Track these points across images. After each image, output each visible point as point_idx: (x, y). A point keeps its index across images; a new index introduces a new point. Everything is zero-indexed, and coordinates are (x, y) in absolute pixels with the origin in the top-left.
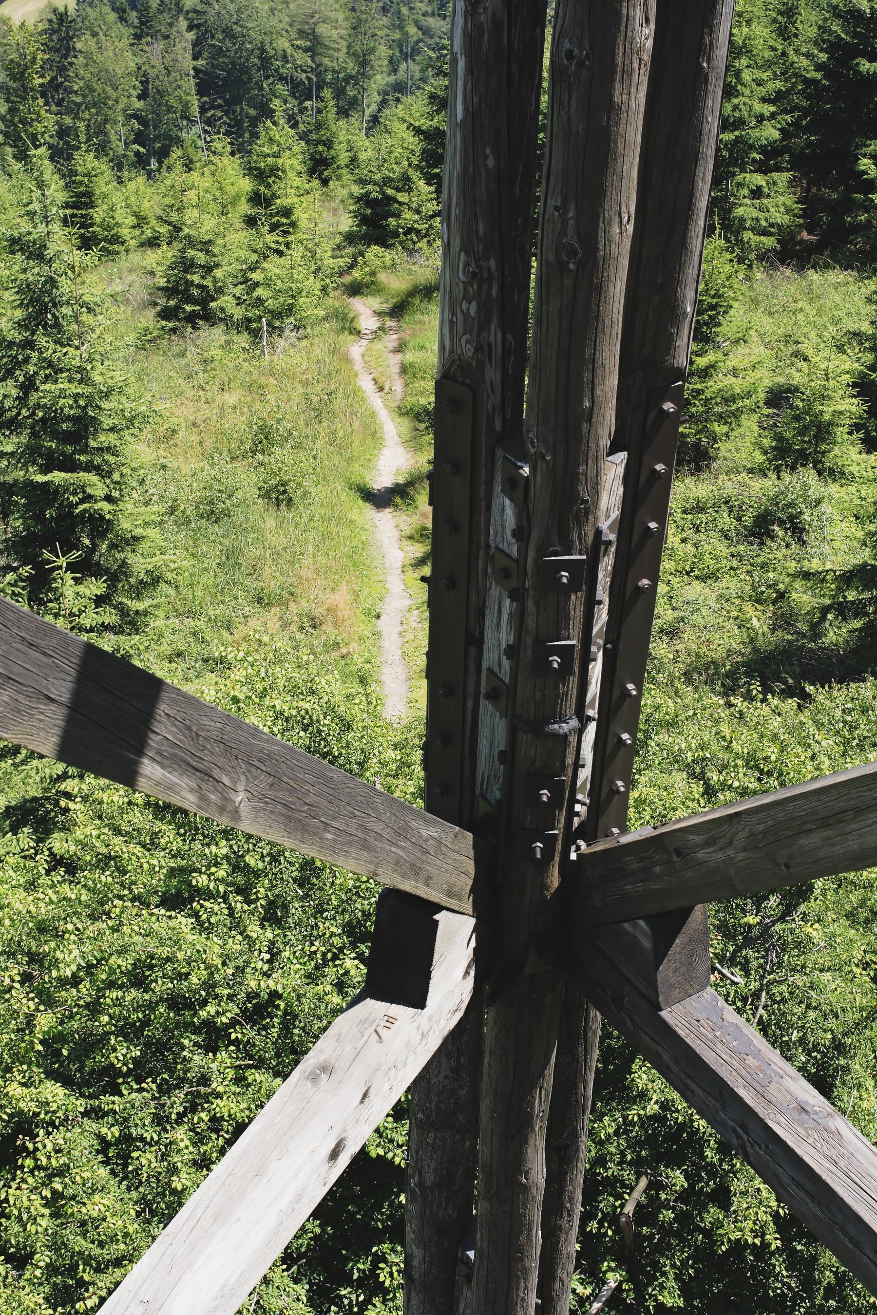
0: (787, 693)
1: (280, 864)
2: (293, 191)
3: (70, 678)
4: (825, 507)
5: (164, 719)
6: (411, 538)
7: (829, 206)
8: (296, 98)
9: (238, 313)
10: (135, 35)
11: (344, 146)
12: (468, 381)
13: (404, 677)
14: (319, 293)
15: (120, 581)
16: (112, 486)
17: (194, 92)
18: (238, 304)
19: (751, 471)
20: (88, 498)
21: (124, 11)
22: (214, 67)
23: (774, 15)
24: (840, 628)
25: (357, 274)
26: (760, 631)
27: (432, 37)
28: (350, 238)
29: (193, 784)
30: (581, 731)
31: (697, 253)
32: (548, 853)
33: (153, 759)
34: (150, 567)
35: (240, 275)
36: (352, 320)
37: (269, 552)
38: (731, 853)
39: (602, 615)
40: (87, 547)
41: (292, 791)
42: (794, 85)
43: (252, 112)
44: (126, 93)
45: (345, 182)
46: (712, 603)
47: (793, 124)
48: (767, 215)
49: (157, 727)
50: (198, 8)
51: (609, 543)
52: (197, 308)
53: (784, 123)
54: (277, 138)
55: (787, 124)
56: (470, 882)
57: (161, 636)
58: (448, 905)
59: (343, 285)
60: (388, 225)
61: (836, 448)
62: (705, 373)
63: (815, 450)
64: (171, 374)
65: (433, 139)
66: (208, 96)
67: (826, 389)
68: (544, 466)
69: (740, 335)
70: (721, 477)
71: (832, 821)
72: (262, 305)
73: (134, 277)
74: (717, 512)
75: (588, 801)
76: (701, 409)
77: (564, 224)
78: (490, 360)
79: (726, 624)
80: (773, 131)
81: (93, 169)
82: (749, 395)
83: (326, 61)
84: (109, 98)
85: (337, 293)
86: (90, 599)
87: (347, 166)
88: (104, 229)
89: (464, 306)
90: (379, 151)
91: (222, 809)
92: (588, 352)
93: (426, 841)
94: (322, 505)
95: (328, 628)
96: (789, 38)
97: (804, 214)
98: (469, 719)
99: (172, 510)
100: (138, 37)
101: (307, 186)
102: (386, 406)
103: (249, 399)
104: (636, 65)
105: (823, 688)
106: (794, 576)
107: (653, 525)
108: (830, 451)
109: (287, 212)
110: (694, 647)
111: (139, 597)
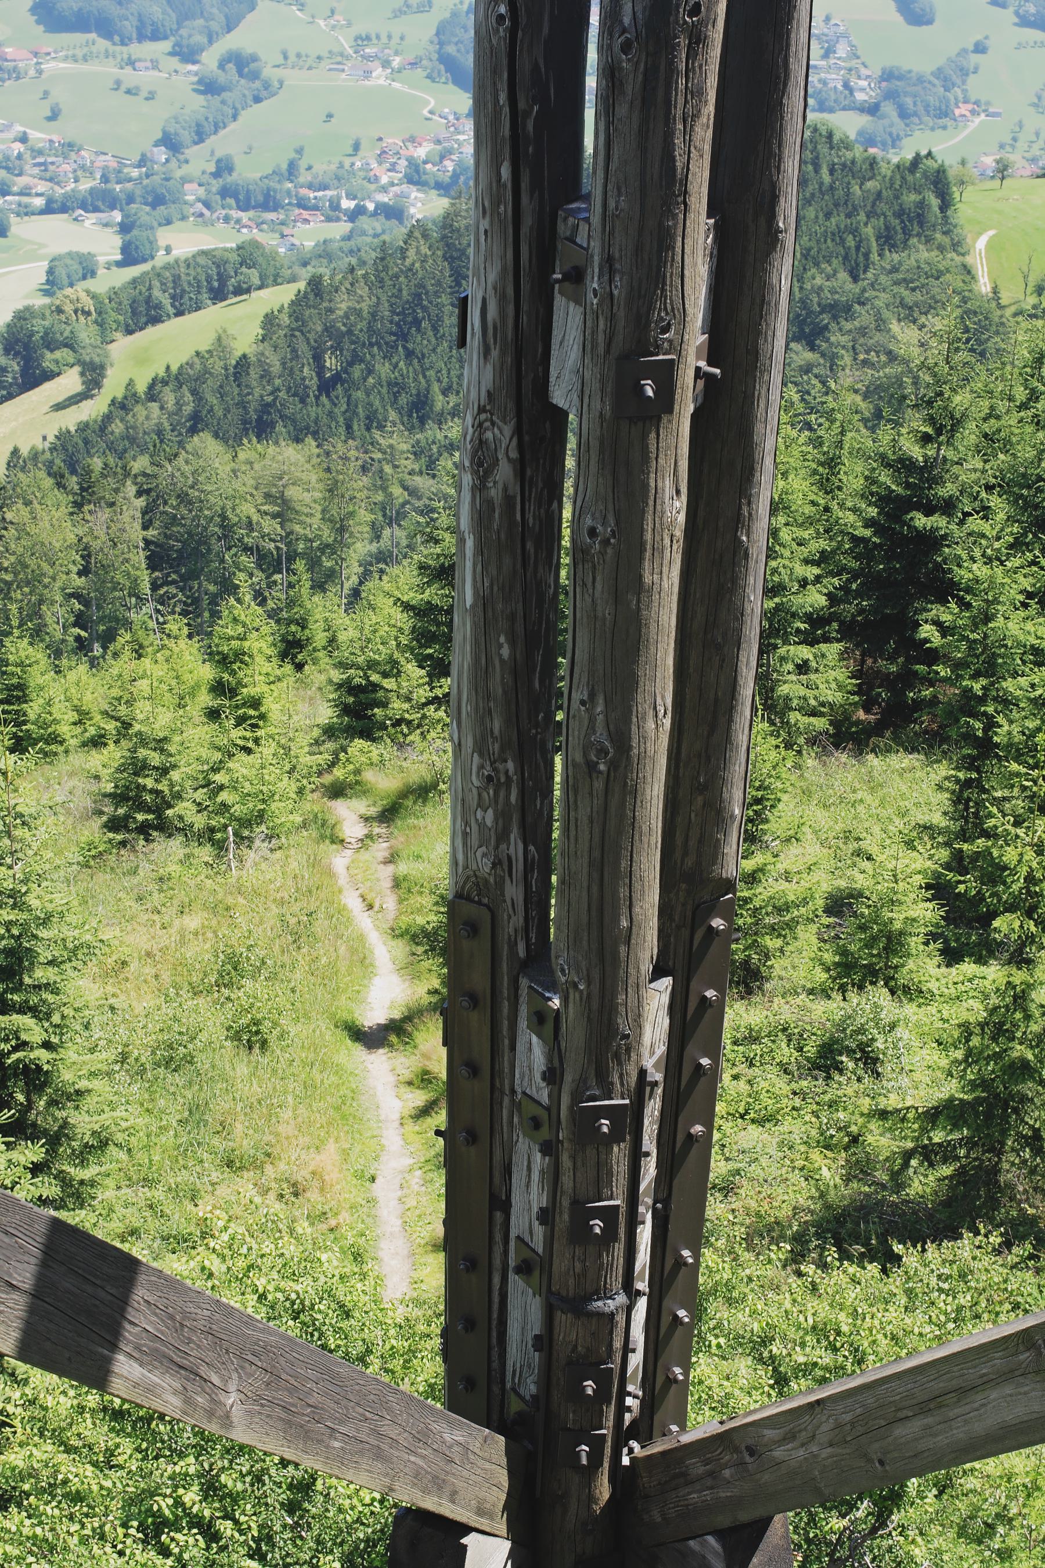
0: (871, 1256)
1: (264, 1484)
2: (262, 678)
3: (33, 1261)
4: (900, 1032)
5: (143, 1307)
6: (410, 1083)
7: (888, 681)
8: (263, 571)
9: (199, 821)
10: (75, 502)
11: (321, 624)
12: (485, 901)
13: (406, 1252)
14: (294, 796)
15: (61, 1145)
16: (51, 1030)
17: (144, 566)
18: (199, 811)
19: (811, 992)
20: (22, 1045)
21: (62, 476)
22: (166, 536)
23: (814, 466)
24: (926, 1176)
25: (339, 773)
26: (832, 1183)
27: (419, 498)
28: (330, 732)
29: (177, 1385)
30: (629, 1309)
31: (744, 748)
32: (596, 1458)
33: (130, 1356)
34: (96, 1127)
35: (201, 777)
36: (334, 826)
37: (240, 1105)
38: (815, 1449)
39: (650, 1169)
40: (21, 1104)
41: (292, 1390)
42: (840, 544)
43: (212, 588)
44: (64, 569)
45: (323, 666)
46: (772, 1150)
47: (841, 588)
48: (816, 692)
49: (131, 1314)
50: (148, 471)
51: (655, 1084)
52: (151, 817)
53: (831, 588)
54: (243, 618)
55: (835, 588)
56: (504, 1497)
57: (111, 1210)
58: (477, 1526)
59: (323, 785)
60: (374, 715)
61: (910, 961)
62: (752, 878)
63: (886, 964)
64: (121, 895)
65: (425, 615)
66: (161, 570)
67: (895, 893)
68: (577, 995)
69: (791, 832)
70: (776, 999)
71: (932, 1406)
72: (228, 811)
73: (74, 782)
74: (773, 1041)
75: (640, 1393)
76: (749, 920)
77: (592, 720)
78: (510, 875)
79: (790, 1176)
80: (818, 596)
81: (27, 657)
82: (805, 902)
83: (297, 528)
84: (44, 575)
85: (316, 795)
86: (25, 1168)
87: (325, 648)
88: (40, 727)
89: (479, 814)
90: (362, 629)
91: (210, 1414)
92: (624, 864)
93: (450, 1447)
94: (303, 1047)
95: (313, 1195)
96: (832, 491)
97: (859, 691)
98: (496, 1299)
99: (124, 1057)
100: (78, 505)
101: (278, 672)
102: (377, 928)
103: (214, 923)
104: (667, 541)
105: (915, 1247)
106: (870, 1115)
107: (705, 1061)
108: (903, 966)
109: (255, 703)
110: (753, 1204)
111: (83, 1163)
